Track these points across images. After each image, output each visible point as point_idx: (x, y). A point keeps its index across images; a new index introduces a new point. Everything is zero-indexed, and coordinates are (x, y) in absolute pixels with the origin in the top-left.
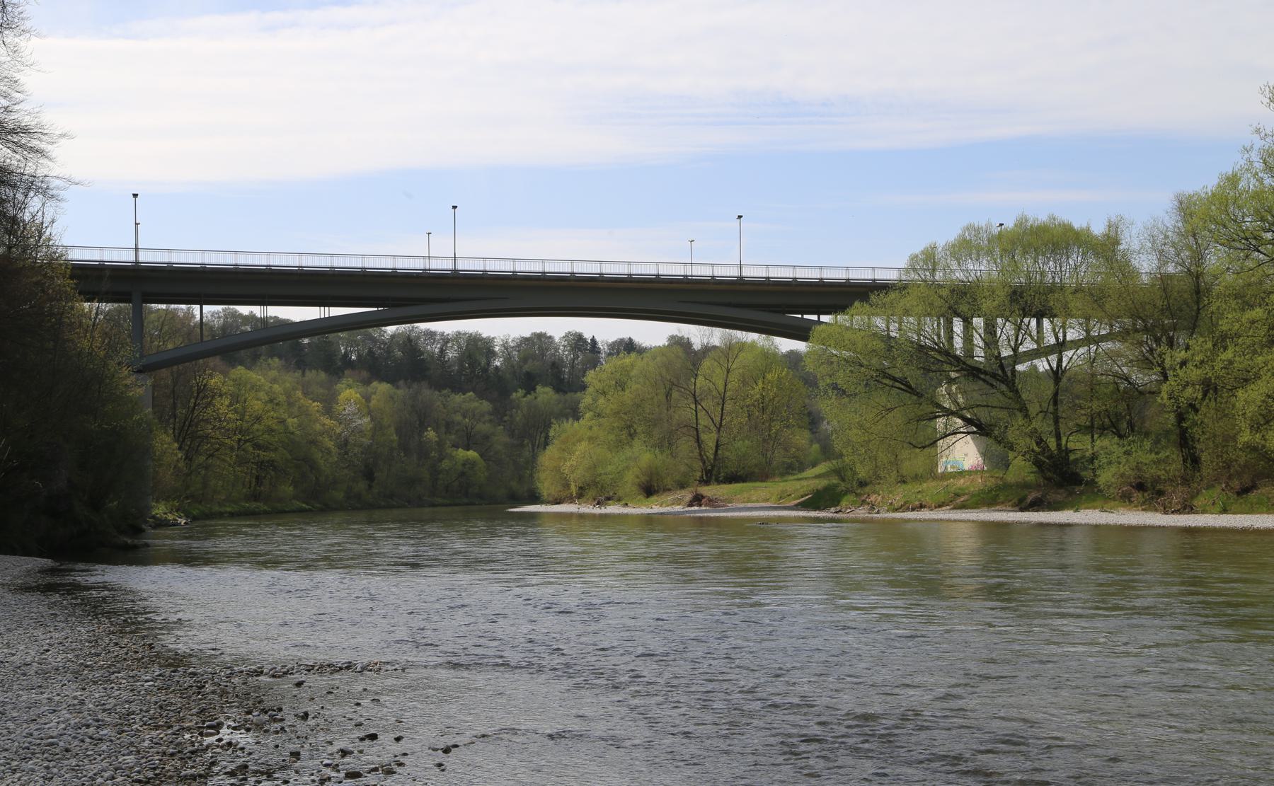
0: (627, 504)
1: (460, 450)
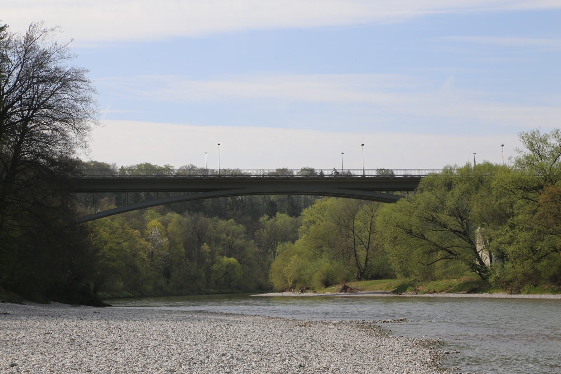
0: (315, 292)
1: (225, 257)
